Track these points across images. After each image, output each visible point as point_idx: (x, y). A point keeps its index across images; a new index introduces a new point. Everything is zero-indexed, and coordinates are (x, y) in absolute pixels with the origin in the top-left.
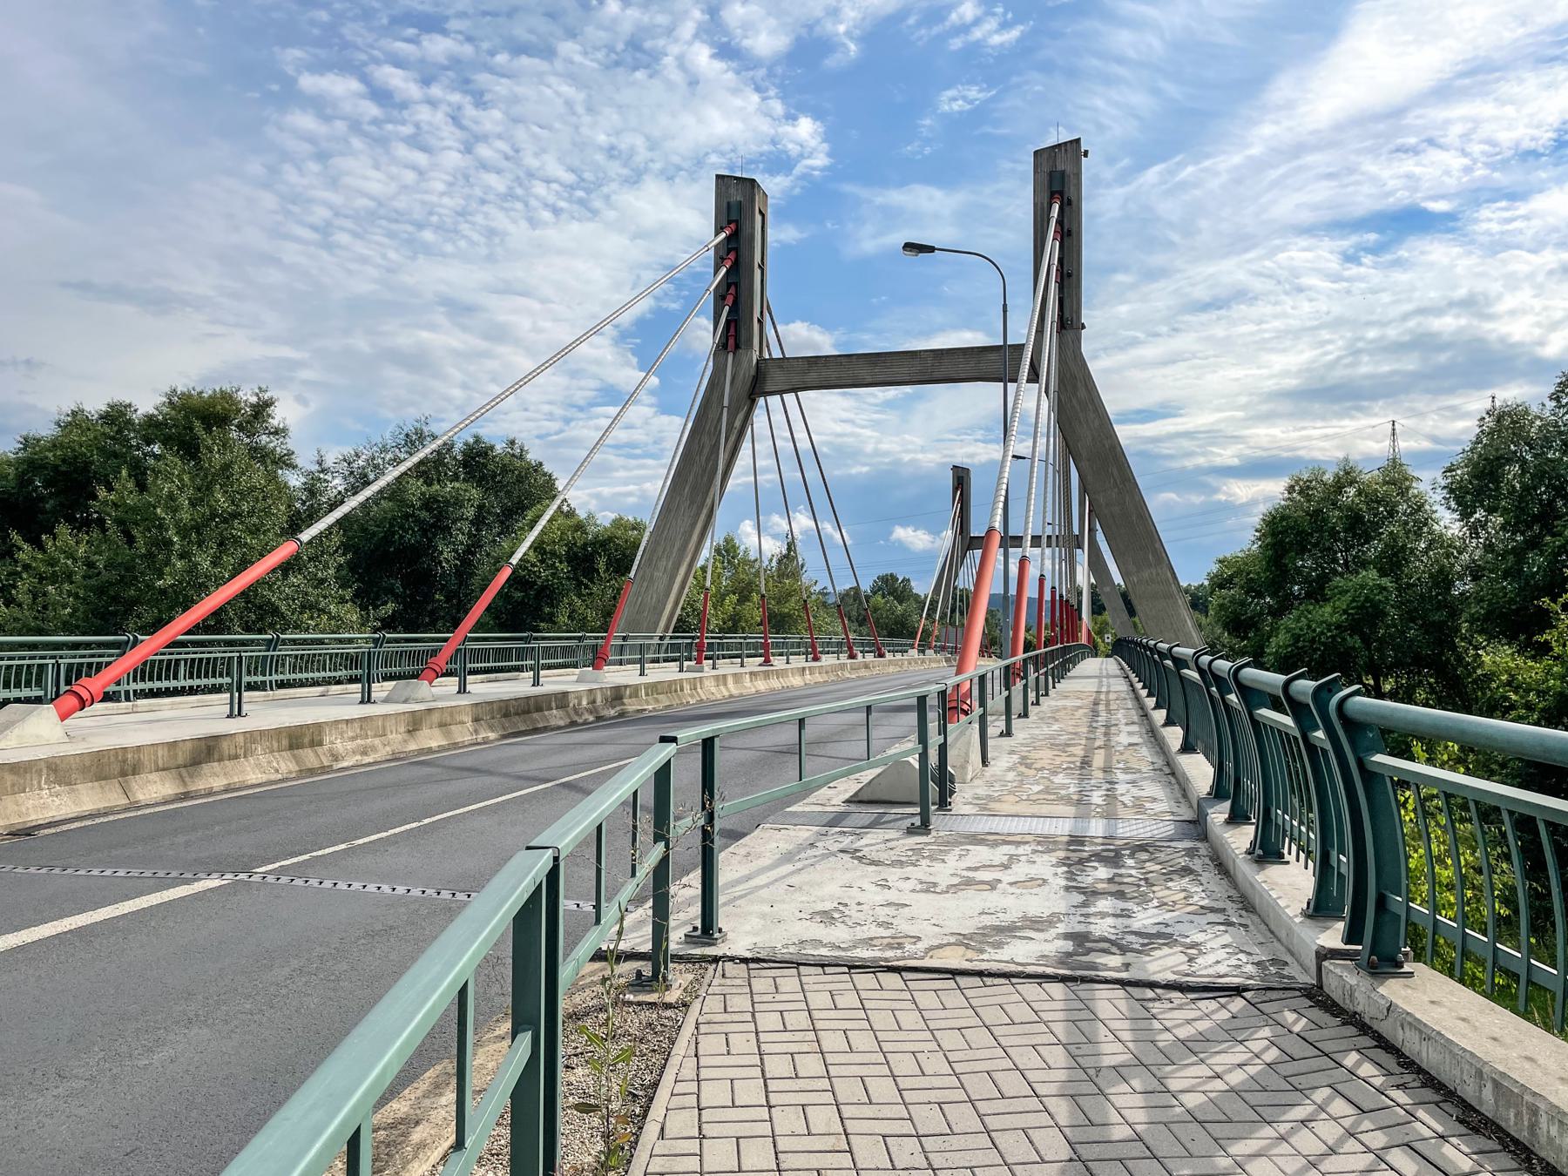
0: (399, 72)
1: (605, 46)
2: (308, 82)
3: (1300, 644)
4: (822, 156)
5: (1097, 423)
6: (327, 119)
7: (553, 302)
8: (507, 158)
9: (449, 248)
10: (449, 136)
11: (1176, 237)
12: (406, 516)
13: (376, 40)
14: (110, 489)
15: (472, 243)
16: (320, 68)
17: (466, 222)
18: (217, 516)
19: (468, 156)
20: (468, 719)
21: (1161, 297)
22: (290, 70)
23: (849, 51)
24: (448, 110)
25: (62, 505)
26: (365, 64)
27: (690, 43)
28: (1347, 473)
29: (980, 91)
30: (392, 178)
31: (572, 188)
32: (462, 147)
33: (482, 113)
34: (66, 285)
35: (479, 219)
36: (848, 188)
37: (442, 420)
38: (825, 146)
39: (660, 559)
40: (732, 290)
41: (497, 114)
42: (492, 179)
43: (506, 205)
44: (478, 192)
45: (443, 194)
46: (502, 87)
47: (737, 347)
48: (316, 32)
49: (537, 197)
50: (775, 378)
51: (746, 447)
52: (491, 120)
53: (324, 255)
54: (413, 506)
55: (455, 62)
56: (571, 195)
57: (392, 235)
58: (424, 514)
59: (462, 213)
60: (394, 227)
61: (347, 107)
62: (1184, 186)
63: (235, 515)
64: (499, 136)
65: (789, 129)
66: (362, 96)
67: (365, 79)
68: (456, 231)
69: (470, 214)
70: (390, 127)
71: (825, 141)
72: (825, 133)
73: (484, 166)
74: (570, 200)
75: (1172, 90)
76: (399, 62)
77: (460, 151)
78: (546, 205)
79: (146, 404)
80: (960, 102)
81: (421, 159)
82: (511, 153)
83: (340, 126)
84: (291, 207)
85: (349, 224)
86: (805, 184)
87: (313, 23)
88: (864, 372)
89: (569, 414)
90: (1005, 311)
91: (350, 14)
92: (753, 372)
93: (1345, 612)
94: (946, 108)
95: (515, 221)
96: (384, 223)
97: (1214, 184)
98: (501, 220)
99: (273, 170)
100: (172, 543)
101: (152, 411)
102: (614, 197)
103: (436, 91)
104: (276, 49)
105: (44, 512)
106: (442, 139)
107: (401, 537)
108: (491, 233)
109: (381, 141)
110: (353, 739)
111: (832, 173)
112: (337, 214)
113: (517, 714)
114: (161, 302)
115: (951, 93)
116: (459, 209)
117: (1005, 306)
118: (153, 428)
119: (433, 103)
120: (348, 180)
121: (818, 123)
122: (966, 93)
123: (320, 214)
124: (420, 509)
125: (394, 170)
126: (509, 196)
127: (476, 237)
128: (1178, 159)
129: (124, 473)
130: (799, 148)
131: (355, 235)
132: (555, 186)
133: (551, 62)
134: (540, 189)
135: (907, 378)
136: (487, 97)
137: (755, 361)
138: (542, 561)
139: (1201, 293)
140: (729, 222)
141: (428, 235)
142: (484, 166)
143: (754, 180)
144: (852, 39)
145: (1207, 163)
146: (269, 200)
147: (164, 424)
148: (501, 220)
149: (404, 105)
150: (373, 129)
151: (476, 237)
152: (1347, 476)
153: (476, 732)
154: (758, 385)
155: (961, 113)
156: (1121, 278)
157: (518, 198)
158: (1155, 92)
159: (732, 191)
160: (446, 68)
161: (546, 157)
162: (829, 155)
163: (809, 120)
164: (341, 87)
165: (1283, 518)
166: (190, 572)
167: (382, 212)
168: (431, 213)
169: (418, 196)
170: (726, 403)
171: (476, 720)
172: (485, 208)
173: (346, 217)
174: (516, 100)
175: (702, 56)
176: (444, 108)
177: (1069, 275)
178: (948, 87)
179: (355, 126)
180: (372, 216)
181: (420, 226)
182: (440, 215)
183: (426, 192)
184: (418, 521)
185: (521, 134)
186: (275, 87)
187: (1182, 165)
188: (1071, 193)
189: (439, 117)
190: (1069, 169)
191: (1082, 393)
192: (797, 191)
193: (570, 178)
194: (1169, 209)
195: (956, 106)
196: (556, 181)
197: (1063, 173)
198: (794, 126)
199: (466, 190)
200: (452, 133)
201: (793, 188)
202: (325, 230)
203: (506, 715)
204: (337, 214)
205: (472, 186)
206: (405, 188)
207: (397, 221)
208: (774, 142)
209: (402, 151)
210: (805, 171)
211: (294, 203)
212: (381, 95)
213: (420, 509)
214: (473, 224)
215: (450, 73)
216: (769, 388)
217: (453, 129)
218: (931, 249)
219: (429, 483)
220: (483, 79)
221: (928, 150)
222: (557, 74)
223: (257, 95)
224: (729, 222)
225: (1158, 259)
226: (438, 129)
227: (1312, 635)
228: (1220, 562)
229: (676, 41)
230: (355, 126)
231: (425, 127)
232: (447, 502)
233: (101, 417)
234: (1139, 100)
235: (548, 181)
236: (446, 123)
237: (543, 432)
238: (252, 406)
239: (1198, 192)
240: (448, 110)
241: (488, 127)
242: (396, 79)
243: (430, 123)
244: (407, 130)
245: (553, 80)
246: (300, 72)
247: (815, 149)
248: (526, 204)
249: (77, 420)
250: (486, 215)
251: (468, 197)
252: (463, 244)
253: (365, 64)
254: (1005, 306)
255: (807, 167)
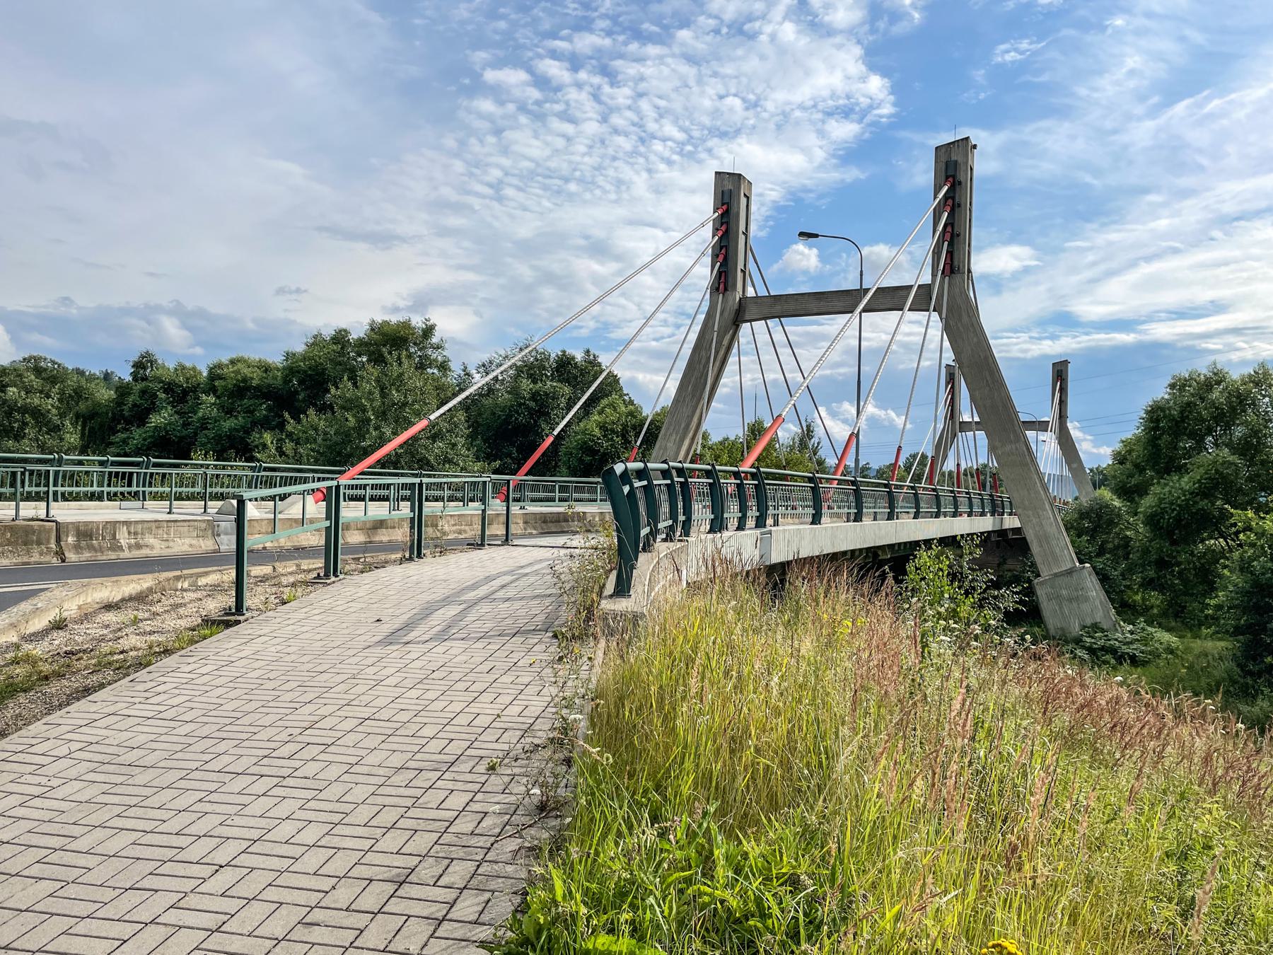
0: (556, 63)
1: (712, 31)
2: (491, 76)
3: (1162, 506)
4: (888, 105)
5: (975, 339)
6: (501, 103)
7: (673, 231)
8: (634, 124)
9: (588, 196)
10: (590, 109)
11: (1204, 161)
12: (520, 405)
13: (540, 41)
14: (337, 388)
15: (605, 192)
16: (498, 64)
17: (602, 175)
18: (395, 404)
19: (604, 125)
20: (521, 522)
21: (1191, 214)
22: (477, 68)
23: (913, 19)
24: (591, 90)
25: (309, 396)
26: (531, 59)
27: (781, 24)
28: (1215, 374)
29: (1031, 43)
30: (547, 144)
31: (683, 144)
32: (600, 118)
33: (616, 90)
34: (320, 229)
35: (611, 172)
36: (903, 134)
37: (581, 327)
38: (892, 98)
39: (671, 435)
40: (723, 251)
41: (626, 91)
42: (620, 140)
43: (631, 160)
44: (611, 151)
45: (584, 155)
46: (632, 70)
47: (726, 289)
48: (497, 37)
49: (656, 154)
50: (751, 311)
51: (733, 359)
52: (622, 95)
53: (495, 205)
54: (524, 398)
55: (599, 53)
56: (682, 150)
57: (545, 188)
58: (532, 404)
59: (599, 168)
60: (548, 181)
61: (517, 93)
62: (1211, 117)
63: (405, 404)
64: (629, 108)
65: (862, 86)
66: (527, 84)
67: (530, 70)
68: (593, 183)
69: (605, 169)
70: (548, 105)
71: (891, 94)
72: (892, 87)
73: (616, 131)
74: (681, 153)
75: (1198, 37)
76: (554, 55)
77: (598, 121)
78: (662, 159)
79: (358, 331)
80: (1012, 54)
81: (569, 128)
82: (636, 119)
83: (511, 107)
84: (474, 170)
85: (515, 181)
86: (873, 129)
87: (495, 32)
88: (813, 306)
89: (680, 322)
90: (861, 275)
91: (522, 22)
92: (736, 307)
93: (1199, 481)
94: (1000, 59)
95: (637, 173)
96: (540, 179)
97: (1240, 114)
98: (627, 173)
99: (462, 143)
100: (371, 420)
101: (362, 335)
102: (715, 151)
103: (582, 75)
104: (468, 52)
105: (298, 400)
106: (585, 112)
107: (517, 419)
108: (619, 183)
109: (540, 118)
110: (453, 525)
111: (899, 121)
112: (506, 174)
113: (551, 522)
114: (382, 239)
115: (1003, 47)
116: (596, 165)
117: (861, 271)
118: (363, 345)
119: (579, 86)
120: (516, 148)
121: (886, 80)
122: (1016, 46)
123: (496, 173)
124: (529, 400)
125: (549, 138)
126: (635, 153)
127: (608, 187)
128: (1205, 93)
129: (345, 378)
130: (869, 101)
131: (519, 189)
132: (670, 143)
133: (669, 46)
134: (658, 146)
135: (843, 309)
136: (620, 77)
137: (738, 299)
138: (604, 436)
139: (1229, 208)
140: (723, 204)
141: (573, 187)
142: (616, 131)
143: (740, 175)
144: (916, 8)
145: (1233, 96)
146: (459, 166)
147: (366, 344)
148: (627, 173)
149: (558, 89)
150: (535, 108)
151: (608, 187)
152: (1217, 379)
153: (525, 529)
154: (739, 316)
155: (1013, 62)
156: (1153, 198)
157: (641, 155)
158: (1182, 39)
159: (726, 182)
160: (591, 58)
161: (664, 121)
162: (895, 105)
163: (878, 77)
164: (514, 77)
165: (1162, 409)
166: (381, 438)
167: (540, 170)
168: (575, 170)
169: (566, 157)
170: (716, 329)
171: (525, 522)
172: (616, 164)
173: (513, 175)
174: (642, 79)
175: (789, 31)
176: (587, 88)
177: (958, 235)
178: (1003, 43)
179: (522, 108)
180: (532, 175)
181: (567, 180)
182: (581, 171)
183: (573, 154)
184: (528, 408)
185: (644, 105)
186: (467, 81)
187: (1209, 99)
188: (961, 177)
189: (583, 96)
190: (960, 159)
191: (965, 319)
192: (867, 135)
193: (680, 136)
194: (1201, 137)
195: (1010, 57)
196: (669, 139)
197: (956, 162)
198: (864, 82)
199: (602, 151)
200: (593, 108)
201: (863, 133)
202: (497, 186)
203: (545, 522)
204: (506, 174)
205: (606, 147)
206: (556, 151)
207: (550, 177)
208: (848, 97)
209: (556, 124)
210: (874, 119)
211: (477, 167)
212: (542, 82)
213: (529, 400)
214: (606, 176)
215: (594, 62)
216: (747, 318)
217: (594, 104)
218: (816, 236)
219: (535, 382)
220: (618, 64)
221: (982, 96)
222: (673, 56)
223: (454, 88)
224: (723, 204)
225: (1185, 182)
226: (583, 105)
227: (1171, 498)
228: (1123, 442)
229: (770, 22)
230: (522, 108)
231: (573, 104)
232: (546, 394)
233: (332, 339)
234: (1167, 46)
235: (664, 140)
236: (589, 100)
237: (658, 335)
238: (423, 330)
239: (1225, 122)
240: (591, 90)
241: (621, 101)
242: (554, 69)
243: (577, 101)
244: (558, 107)
245: (669, 60)
246: (483, 69)
247: (882, 101)
248: (647, 159)
249: (317, 342)
250: (616, 169)
251: (603, 157)
252: (598, 192)
253: (531, 59)
254: (861, 271)
255: (876, 115)
